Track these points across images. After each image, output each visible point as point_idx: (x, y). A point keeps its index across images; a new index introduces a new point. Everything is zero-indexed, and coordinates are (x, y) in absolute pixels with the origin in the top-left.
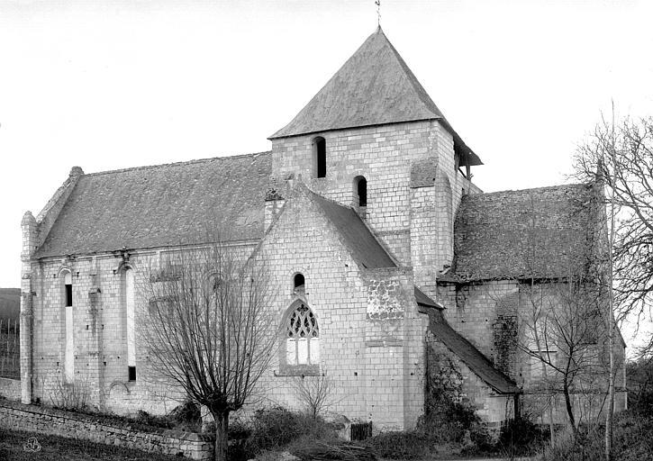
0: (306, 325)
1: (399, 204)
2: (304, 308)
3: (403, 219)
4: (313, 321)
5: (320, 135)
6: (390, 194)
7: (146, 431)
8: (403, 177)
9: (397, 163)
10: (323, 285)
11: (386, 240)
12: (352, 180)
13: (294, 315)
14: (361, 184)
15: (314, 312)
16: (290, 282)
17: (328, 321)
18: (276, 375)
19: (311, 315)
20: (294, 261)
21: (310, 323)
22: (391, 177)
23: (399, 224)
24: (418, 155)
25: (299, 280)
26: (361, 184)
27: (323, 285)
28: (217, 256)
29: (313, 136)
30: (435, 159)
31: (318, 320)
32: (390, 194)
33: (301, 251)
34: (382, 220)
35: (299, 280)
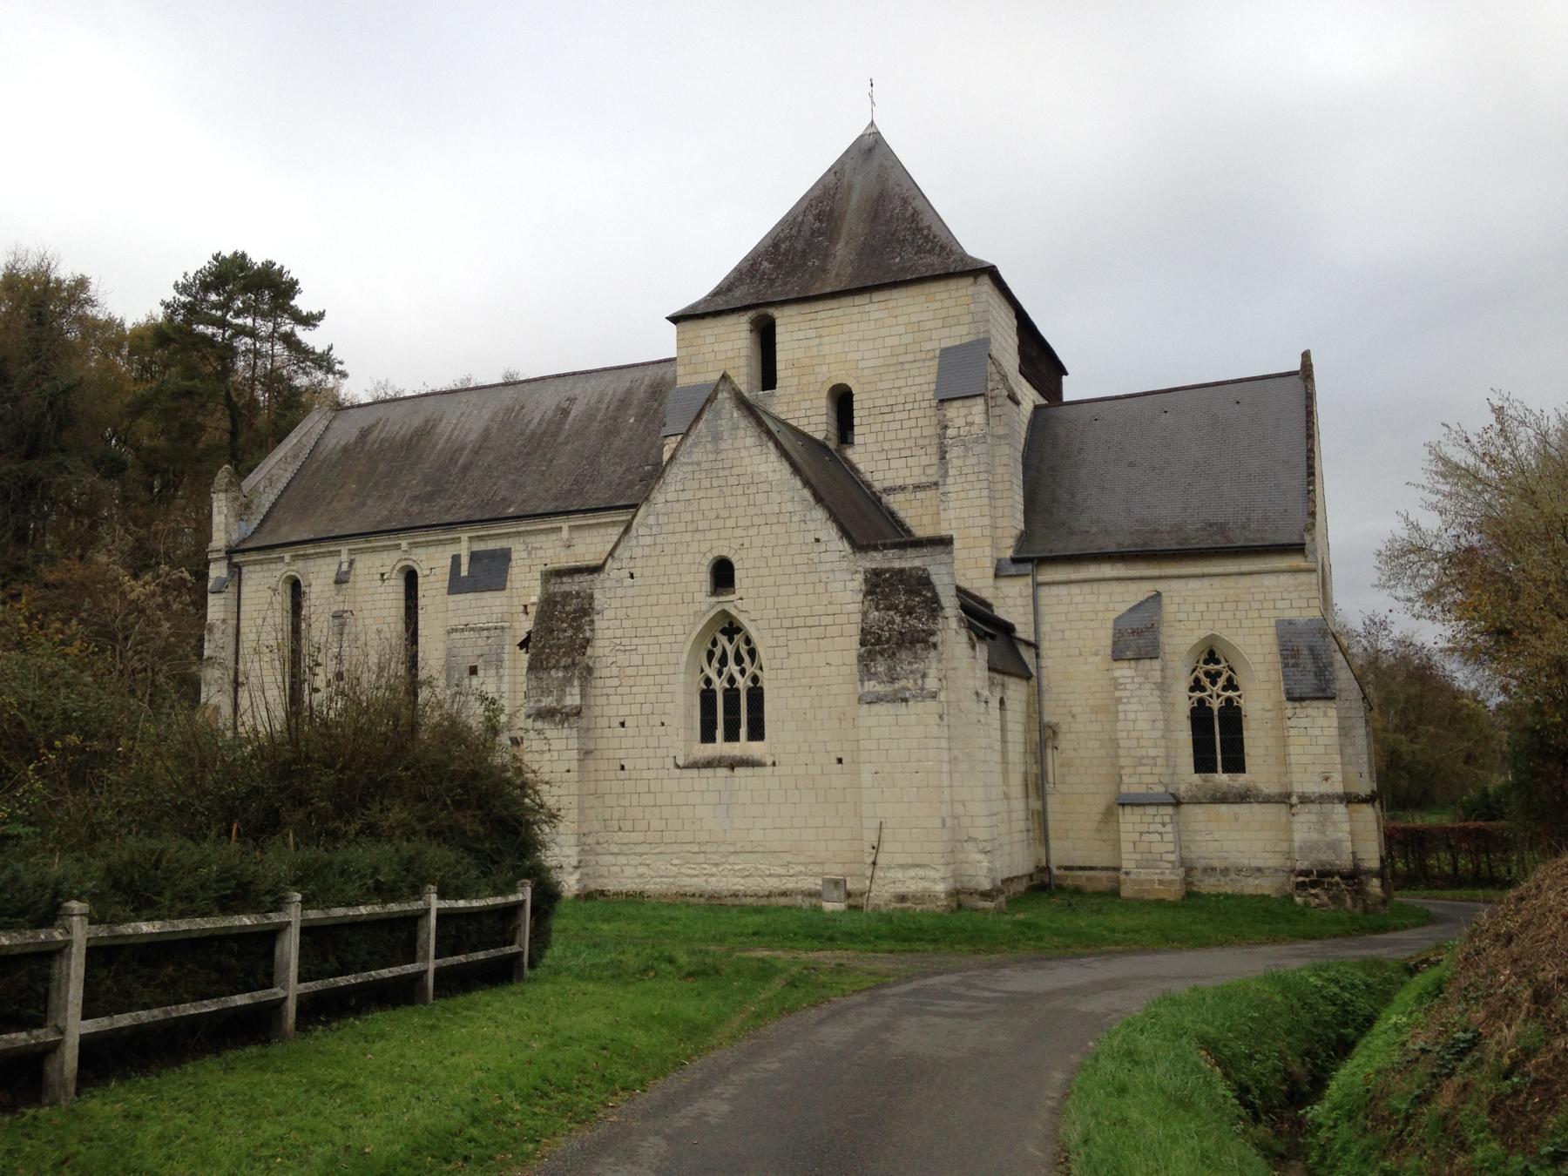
0: (739, 660)
1: (916, 433)
2: (732, 628)
3: (925, 460)
4: (752, 653)
5: (762, 311)
6: (898, 416)
7: (820, 950)
8: (923, 380)
9: (910, 357)
10: (771, 580)
11: (895, 502)
12: (825, 393)
13: (714, 643)
14: (842, 400)
15: (754, 634)
16: (704, 578)
17: (781, 653)
18: (677, 766)
19: (748, 641)
20: (713, 535)
21: (747, 659)
22: (901, 383)
23: (916, 471)
24: (959, 335)
25: (723, 575)
26: (842, 400)
27: (771, 580)
28: (558, 701)
29: (751, 314)
30: (986, 342)
31: (762, 651)
32: (898, 416)
33: (724, 513)
34: (883, 465)
35: (723, 575)
